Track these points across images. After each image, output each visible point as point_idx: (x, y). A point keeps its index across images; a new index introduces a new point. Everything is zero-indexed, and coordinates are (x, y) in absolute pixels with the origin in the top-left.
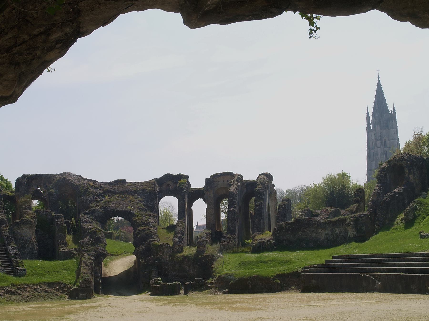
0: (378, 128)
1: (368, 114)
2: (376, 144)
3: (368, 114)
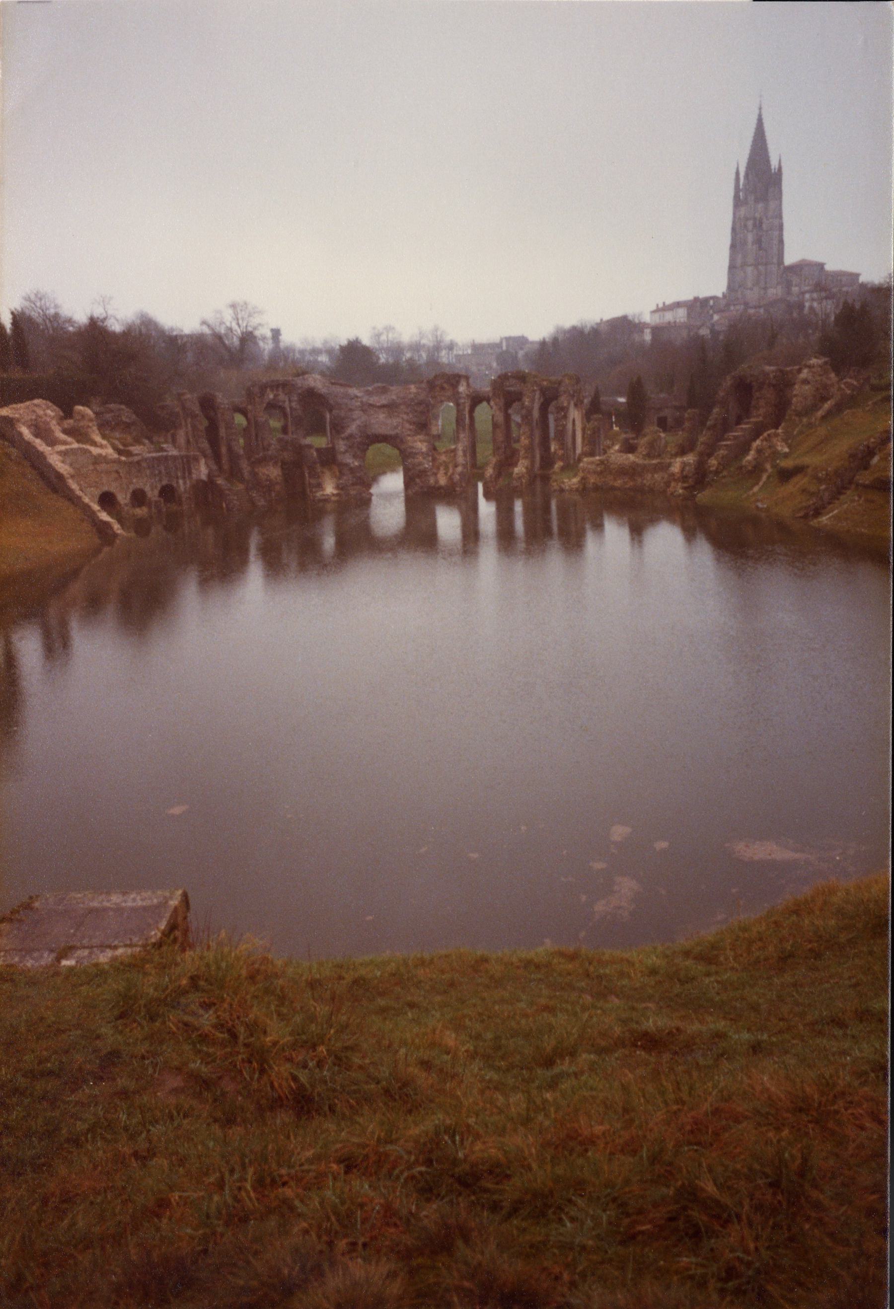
0: (751, 198)
1: (737, 173)
2: (745, 226)
3: (737, 173)
